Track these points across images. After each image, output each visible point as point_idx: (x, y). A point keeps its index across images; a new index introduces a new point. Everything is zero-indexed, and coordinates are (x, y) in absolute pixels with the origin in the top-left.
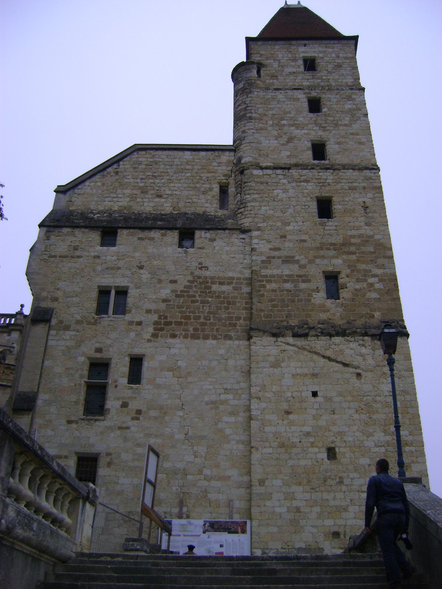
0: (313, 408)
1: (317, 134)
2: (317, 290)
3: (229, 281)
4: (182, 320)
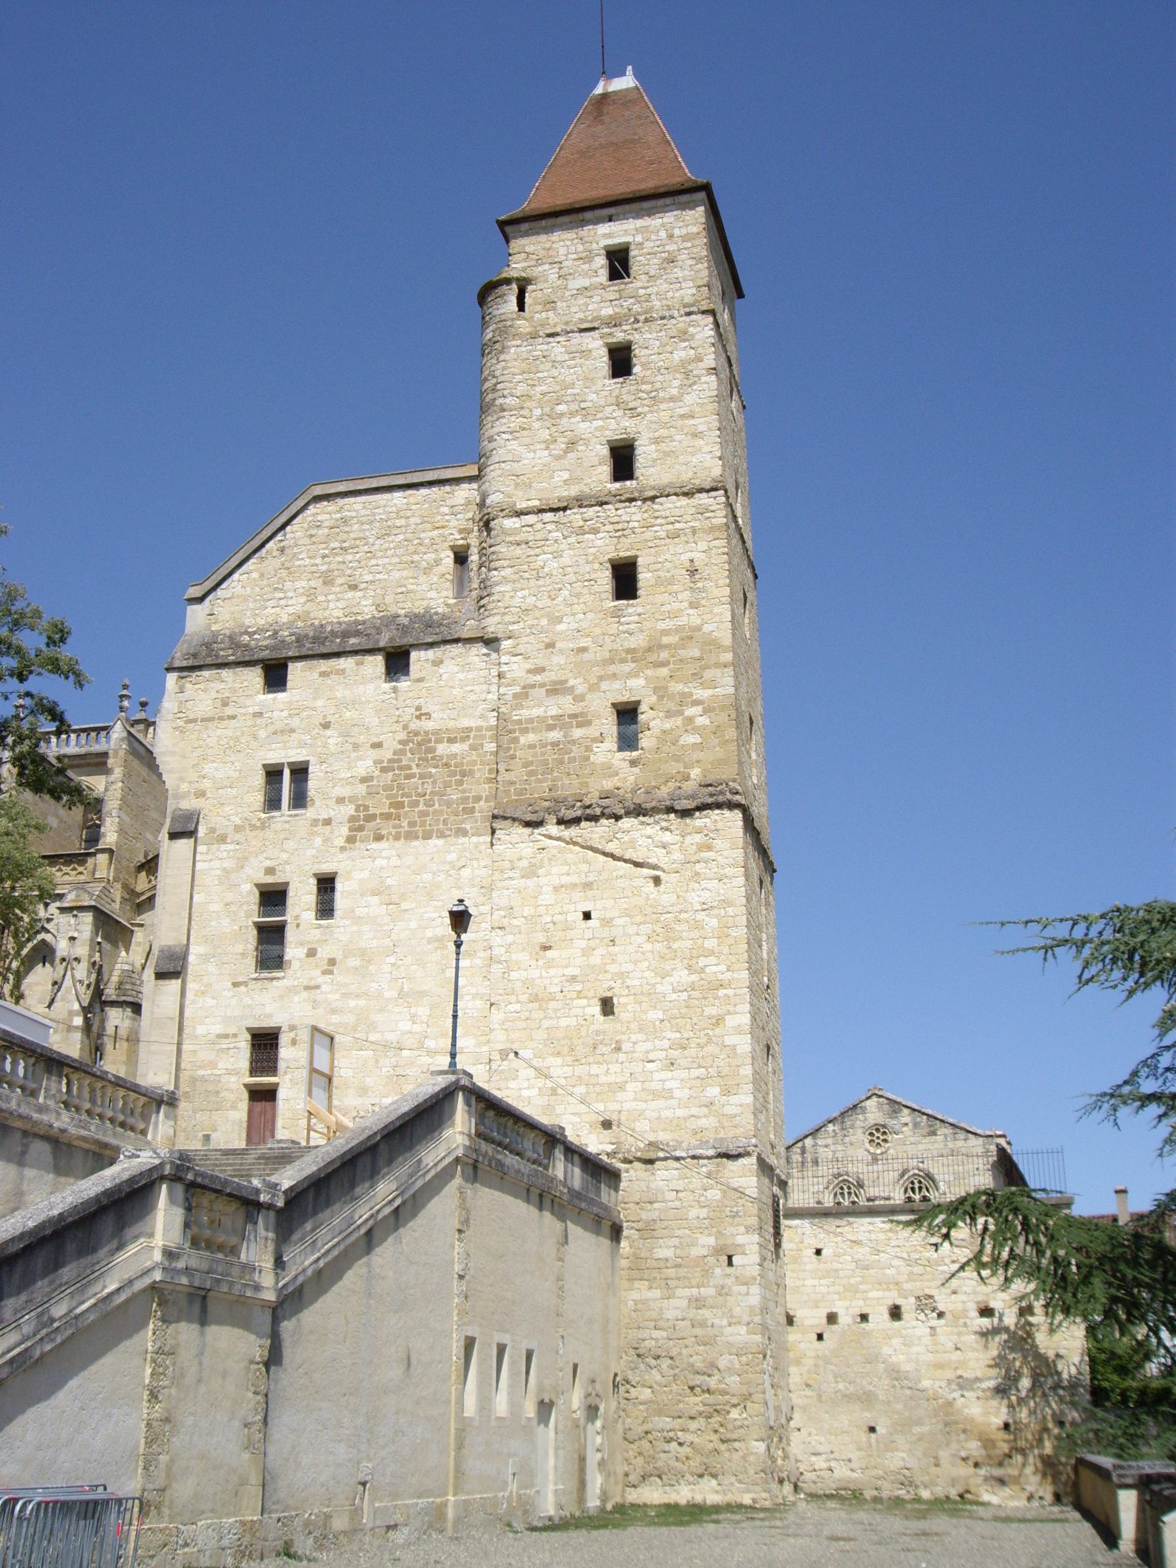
1: (618, 427)
2: (601, 739)
3: (463, 735)
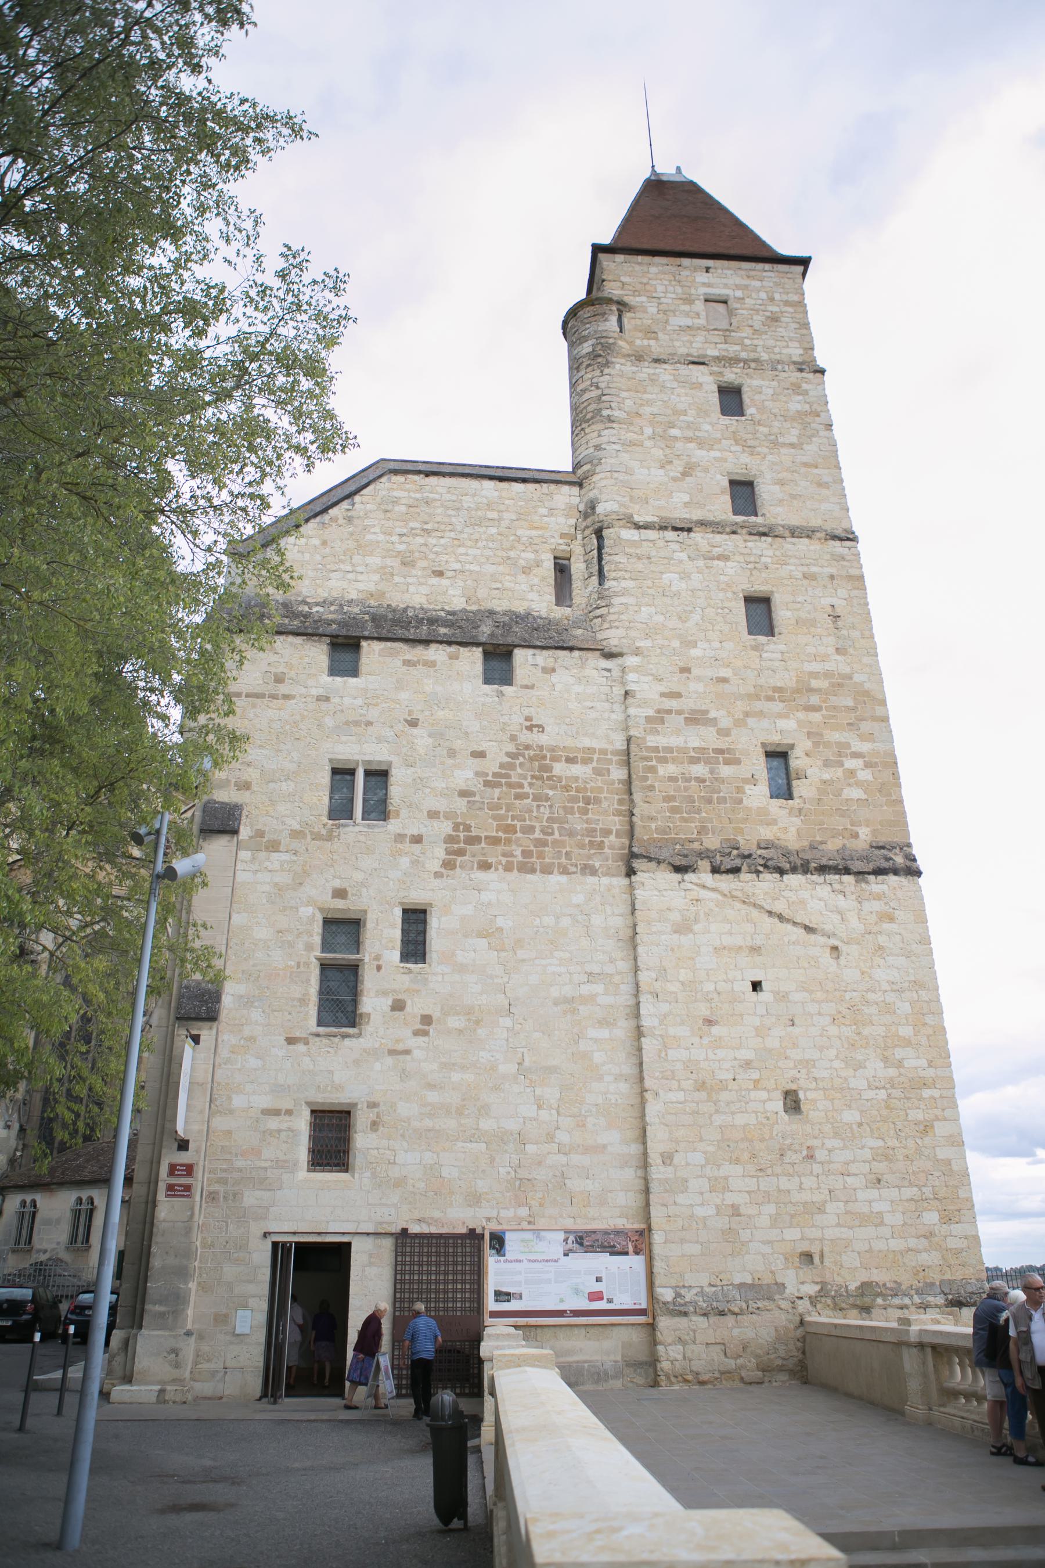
0: (755, 1014)
2: (753, 780)
3: (585, 756)
4: (500, 834)
